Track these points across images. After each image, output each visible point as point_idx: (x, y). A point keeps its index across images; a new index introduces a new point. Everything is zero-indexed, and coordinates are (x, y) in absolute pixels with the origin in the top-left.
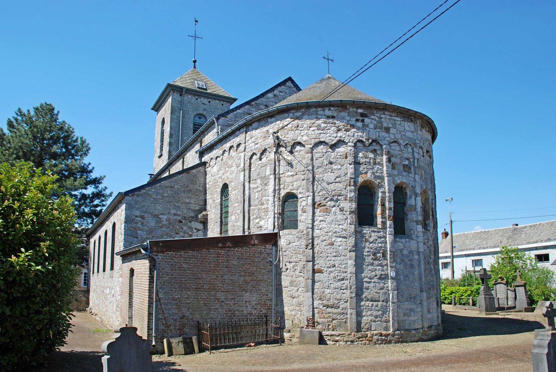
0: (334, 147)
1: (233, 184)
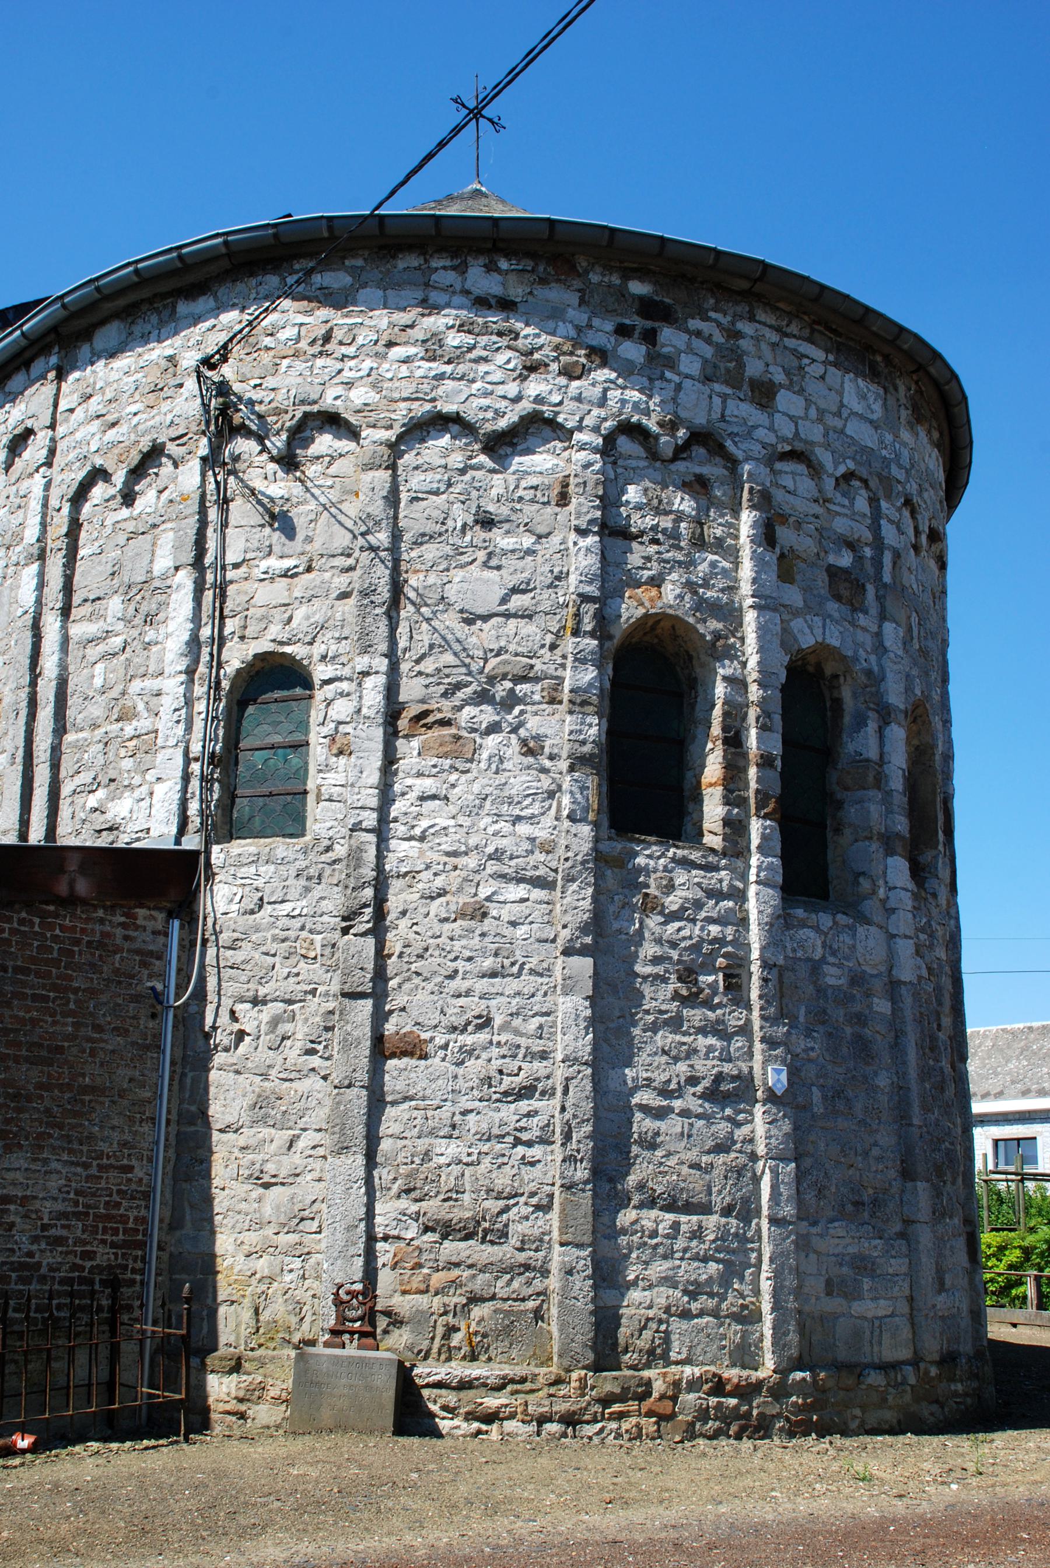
0: (502, 445)
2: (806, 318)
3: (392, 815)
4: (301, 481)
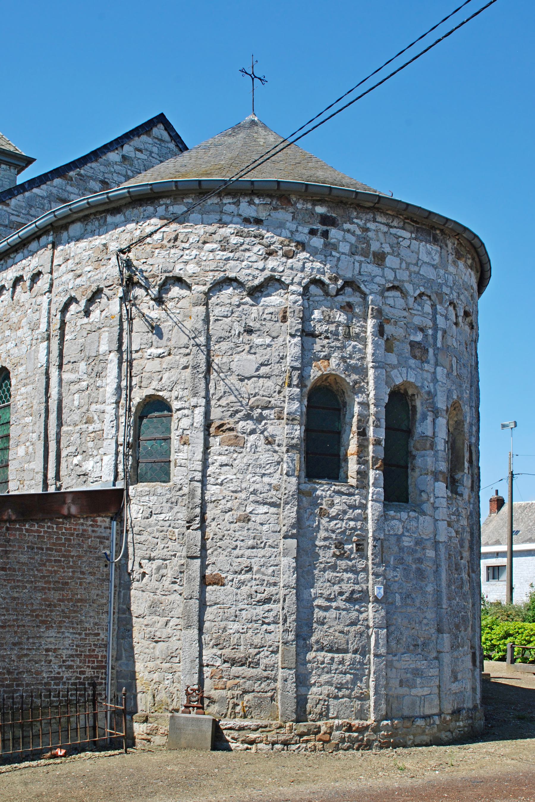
0: (257, 292)
1: (21, 369)
2: (401, 217)
3: (208, 473)
4: (165, 310)
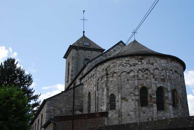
1: (92, 92)
